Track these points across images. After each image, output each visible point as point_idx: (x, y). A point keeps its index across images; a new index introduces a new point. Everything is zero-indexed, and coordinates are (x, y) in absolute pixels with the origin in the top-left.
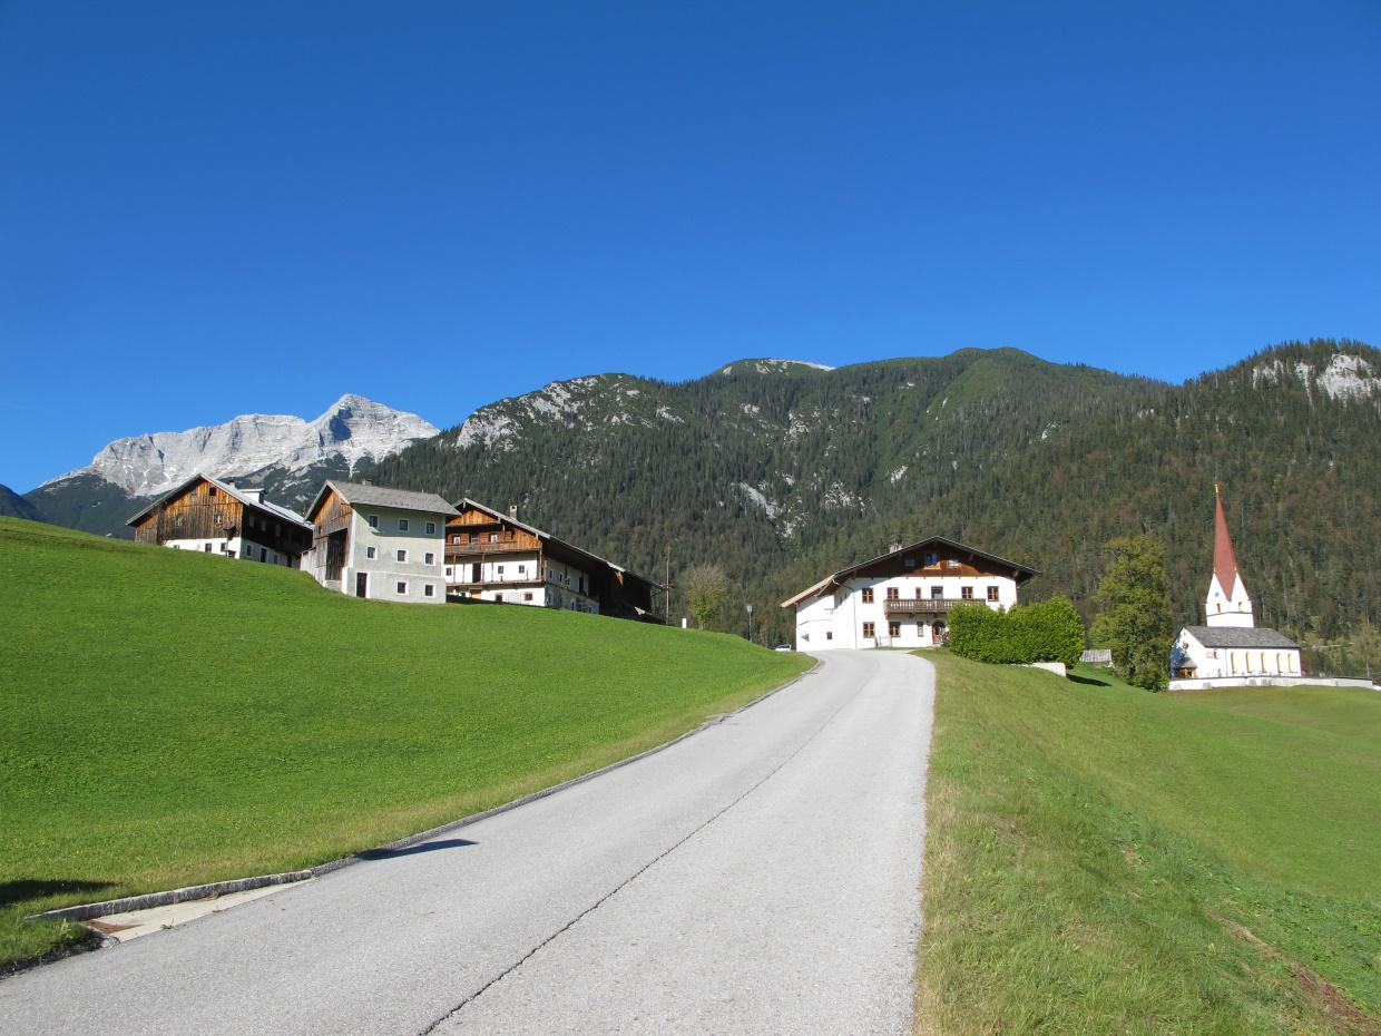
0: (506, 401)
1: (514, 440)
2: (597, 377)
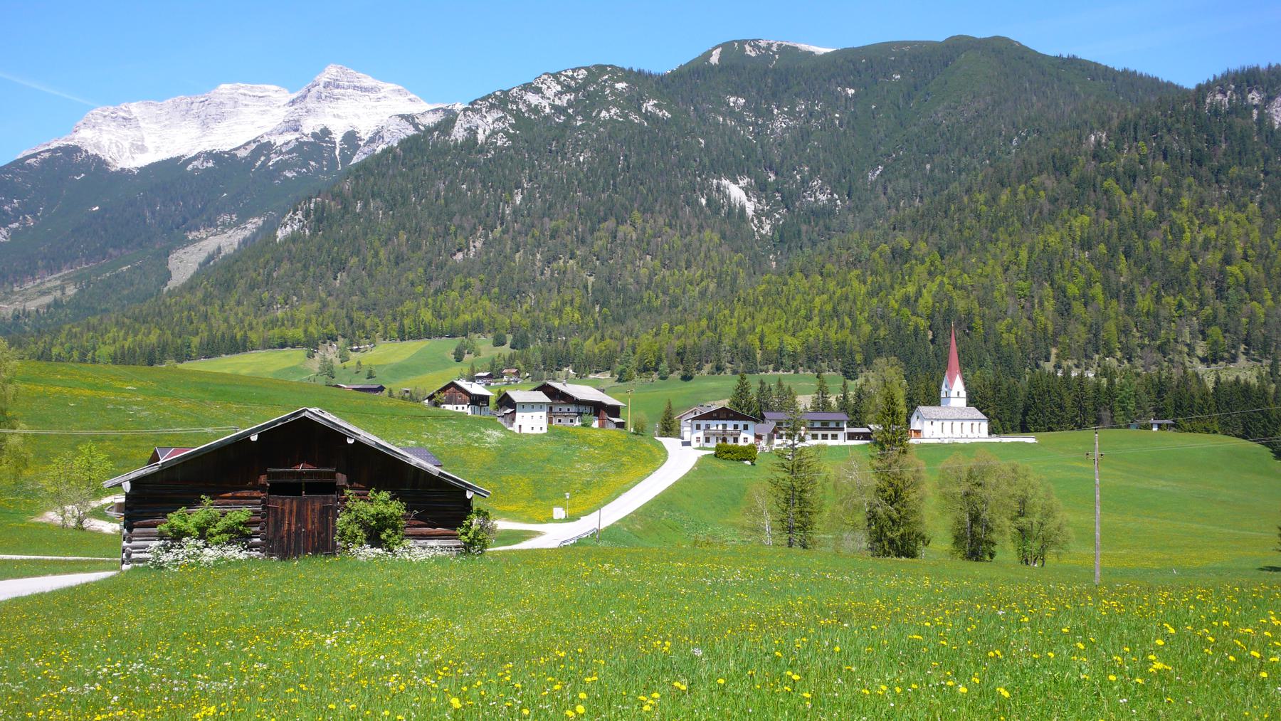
0: (498, 93)
1: (507, 133)
2: (587, 69)
